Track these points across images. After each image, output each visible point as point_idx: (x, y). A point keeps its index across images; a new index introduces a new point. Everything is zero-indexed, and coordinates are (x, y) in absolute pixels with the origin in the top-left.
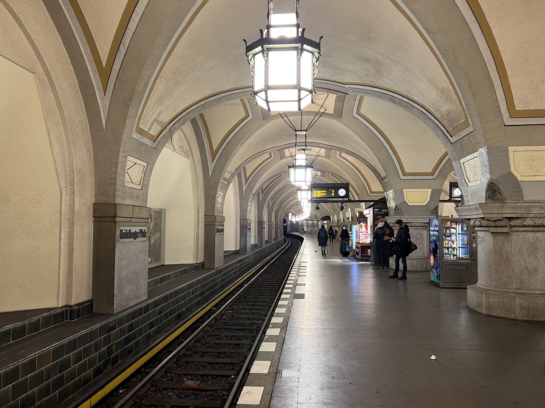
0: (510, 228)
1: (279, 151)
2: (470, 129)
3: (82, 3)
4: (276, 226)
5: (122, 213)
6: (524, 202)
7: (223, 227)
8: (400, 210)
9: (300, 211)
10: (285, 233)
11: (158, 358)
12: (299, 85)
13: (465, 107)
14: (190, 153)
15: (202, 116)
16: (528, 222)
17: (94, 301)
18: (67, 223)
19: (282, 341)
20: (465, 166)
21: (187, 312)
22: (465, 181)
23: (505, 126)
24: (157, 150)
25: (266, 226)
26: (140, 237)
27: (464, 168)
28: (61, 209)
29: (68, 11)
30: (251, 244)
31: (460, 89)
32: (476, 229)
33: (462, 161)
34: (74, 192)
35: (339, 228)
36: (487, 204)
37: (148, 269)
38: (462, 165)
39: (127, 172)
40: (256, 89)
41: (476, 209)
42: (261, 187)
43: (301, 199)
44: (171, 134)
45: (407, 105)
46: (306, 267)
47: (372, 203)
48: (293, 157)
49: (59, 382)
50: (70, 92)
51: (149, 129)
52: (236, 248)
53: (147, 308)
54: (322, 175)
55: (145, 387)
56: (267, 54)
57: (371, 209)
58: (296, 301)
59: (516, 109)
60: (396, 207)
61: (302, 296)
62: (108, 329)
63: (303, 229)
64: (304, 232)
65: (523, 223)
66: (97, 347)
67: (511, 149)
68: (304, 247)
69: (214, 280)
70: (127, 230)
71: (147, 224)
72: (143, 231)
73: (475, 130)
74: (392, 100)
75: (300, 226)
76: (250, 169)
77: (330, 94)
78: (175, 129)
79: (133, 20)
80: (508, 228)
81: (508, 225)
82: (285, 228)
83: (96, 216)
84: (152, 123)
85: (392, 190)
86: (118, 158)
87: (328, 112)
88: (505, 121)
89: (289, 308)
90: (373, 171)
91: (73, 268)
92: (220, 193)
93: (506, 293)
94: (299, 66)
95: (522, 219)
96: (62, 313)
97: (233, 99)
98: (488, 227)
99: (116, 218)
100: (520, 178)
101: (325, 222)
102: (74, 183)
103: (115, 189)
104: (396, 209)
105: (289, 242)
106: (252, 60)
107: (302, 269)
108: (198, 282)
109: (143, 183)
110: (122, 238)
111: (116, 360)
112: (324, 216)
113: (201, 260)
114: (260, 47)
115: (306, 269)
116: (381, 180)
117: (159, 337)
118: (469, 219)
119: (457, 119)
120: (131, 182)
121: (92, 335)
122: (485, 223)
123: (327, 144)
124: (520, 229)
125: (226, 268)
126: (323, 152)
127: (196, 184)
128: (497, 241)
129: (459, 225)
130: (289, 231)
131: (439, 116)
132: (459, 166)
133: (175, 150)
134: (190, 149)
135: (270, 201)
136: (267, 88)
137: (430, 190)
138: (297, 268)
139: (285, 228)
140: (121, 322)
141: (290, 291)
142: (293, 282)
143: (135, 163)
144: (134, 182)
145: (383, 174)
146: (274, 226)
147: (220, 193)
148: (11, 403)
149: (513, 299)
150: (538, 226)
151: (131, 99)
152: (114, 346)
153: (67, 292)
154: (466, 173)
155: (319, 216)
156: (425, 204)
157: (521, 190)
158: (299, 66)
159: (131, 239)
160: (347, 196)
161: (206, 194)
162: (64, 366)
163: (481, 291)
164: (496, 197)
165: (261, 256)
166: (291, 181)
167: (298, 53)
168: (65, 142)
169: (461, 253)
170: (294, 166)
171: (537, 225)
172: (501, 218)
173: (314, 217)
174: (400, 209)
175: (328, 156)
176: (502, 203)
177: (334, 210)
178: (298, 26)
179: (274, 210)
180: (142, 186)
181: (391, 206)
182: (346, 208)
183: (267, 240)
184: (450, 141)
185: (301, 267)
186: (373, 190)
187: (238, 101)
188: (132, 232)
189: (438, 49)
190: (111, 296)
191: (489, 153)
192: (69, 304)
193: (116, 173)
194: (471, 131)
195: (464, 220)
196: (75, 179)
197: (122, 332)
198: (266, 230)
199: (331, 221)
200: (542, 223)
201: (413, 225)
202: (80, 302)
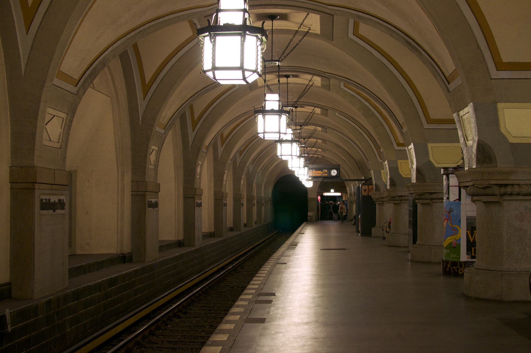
15: (135, 46)
24: (79, 96)
25: (229, 201)
39: (46, 128)
42: (220, 134)
54: (322, 114)
72: (62, 201)
92: (153, 147)
94: (280, 123)
126: (317, 81)
135: (238, 156)
143: (53, 116)
144: (52, 140)
148: (4, 346)
158: (280, 123)
159: (51, 211)
166: (278, 155)
167: (279, 117)
191: (476, 110)
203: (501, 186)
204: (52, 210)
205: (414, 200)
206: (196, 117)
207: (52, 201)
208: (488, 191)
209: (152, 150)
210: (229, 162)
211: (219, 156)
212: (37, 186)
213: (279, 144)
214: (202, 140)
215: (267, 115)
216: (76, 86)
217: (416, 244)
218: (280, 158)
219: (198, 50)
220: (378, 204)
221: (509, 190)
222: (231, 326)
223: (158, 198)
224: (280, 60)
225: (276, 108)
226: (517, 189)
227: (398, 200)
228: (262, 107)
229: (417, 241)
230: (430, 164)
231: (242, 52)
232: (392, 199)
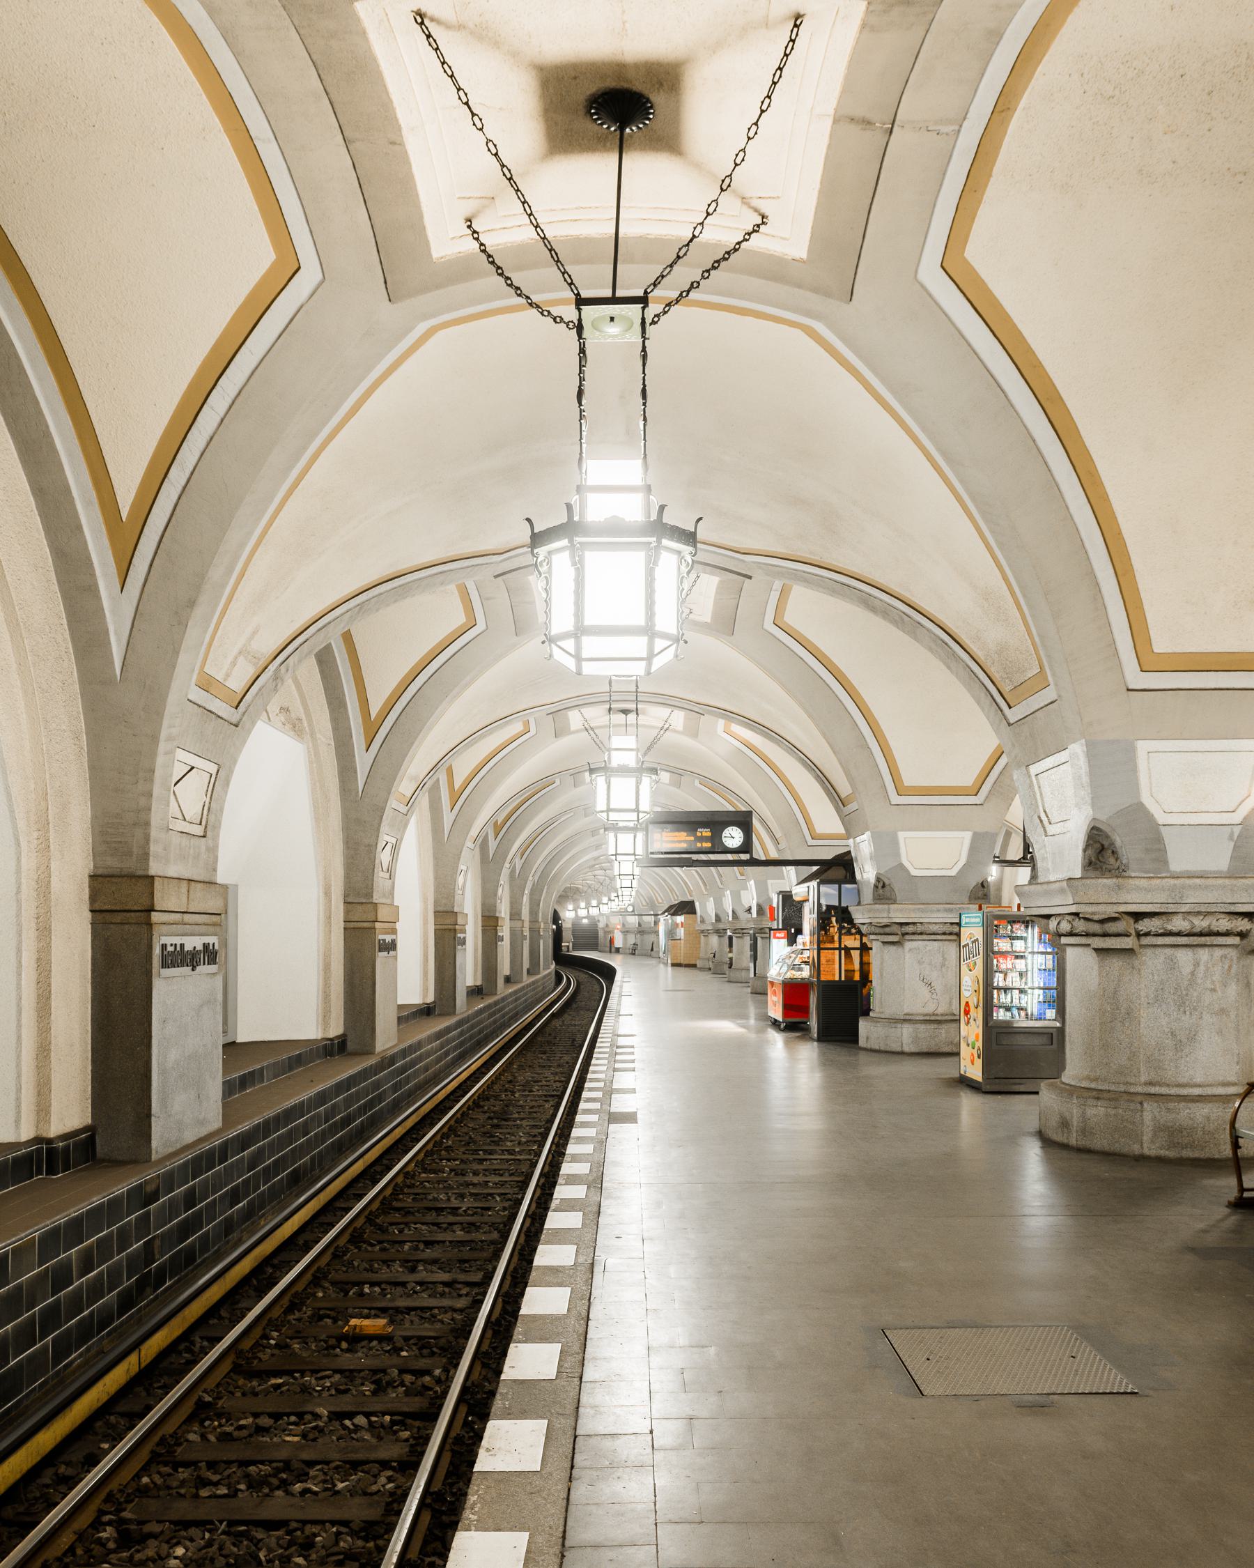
0: (1136, 938)
1: (551, 716)
2: (1049, 694)
3: (79, 361)
4: (534, 932)
5: (167, 898)
6: (1168, 875)
7: (393, 937)
8: (887, 888)
9: (607, 887)
10: (561, 958)
11: (265, 1276)
12: (653, 625)
13: (1037, 639)
14: (305, 724)
15: (348, 638)
16: (1178, 924)
17: (100, 1130)
18: (33, 925)
19: (595, 1209)
20: (1041, 783)
21: (312, 1169)
22: (1041, 821)
23: (1128, 690)
25: (505, 931)
26: (204, 964)
27: (1040, 787)
28: (18, 892)
29: (40, 379)
30: (400, 1002)
31: (1024, 596)
32: (1064, 940)
33: (1034, 769)
34: (49, 847)
35: (722, 939)
36: (1084, 881)
37: (224, 1046)
38: (1034, 778)
40: (555, 630)
41: (1062, 891)
44: (277, 685)
45: (902, 620)
46: (633, 1047)
47: (815, 868)
48: (591, 732)
49: (51, 1318)
50: (35, 583)
51: (228, 675)
52: (425, 995)
53: (224, 1151)
55: (252, 1335)
57: (814, 884)
58: (612, 1127)
59: (1155, 651)
60: (878, 880)
61: (630, 1118)
62: (143, 1196)
63: (611, 941)
64: (613, 950)
65: (1165, 925)
66: (124, 1239)
67: (1142, 747)
68: (620, 995)
69: (377, 1085)
70: (176, 945)
71: (218, 928)
72: (211, 948)
73: (1059, 696)
74: (867, 603)
75: (601, 934)
76: (463, 767)
77: (702, 575)
78: (287, 670)
79: (212, 408)
80: (1132, 937)
81: (1133, 932)
82: (558, 936)
83: (97, 909)
84: (236, 658)
85: (868, 833)
86: (153, 755)
87: (697, 618)
89: (601, 1144)
90: (817, 778)
91: (50, 1043)
92: (387, 838)
93: (1125, 1095)
95: (1164, 917)
96: (29, 1156)
97: (442, 584)
98: (1087, 935)
99: (153, 913)
100: (1161, 818)
101: (680, 919)
102: (48, 824)
103: (147, 840)
104: (877, 887)
105: (571, 978)
106: (545, 564)
107: (621, 1054)
108: (340, 1087)
109: (207, 819)
110: (164, 965)
111: (161, 1276)
112: (677, 902)
113: (336, 1029)
114: (566, 540)
115: (633, 1053)
116: (840, 803)
117: (262, 1223)
118: (1048, 917)
119: (1021, 666)
120: (181, 817)
121: (112, 1209)
122: (1080, 926)
123: (691, 699)
124: (1160, 941)
125: (404, 1053)
126: (678, 719)
127: (319, 816)
128: (1108, 969)
129: (1033, 927)
130: (568, 947)
131: (980, 654)
132: (1028, 781)
134: (305, 713)
136: (580, 631)
137: (967, 836)
138: (608, 1050)
139: (558, 936)
140: (169, 1181)
141: (597, 1106)
142: (601, 1085)
143: (190, 768)
145: (844, 789)
146: (527, 933)
147: (386, 837)
149: (1139, 1108)
150: (1201, 934)
151: (192, 604)
152: (158, 1242)
153: (38, 1104)
154: (1042, 799)
156: (953, 873)
157: (1162, 846)
159: (185, 968)
160: (746, 847)
161: (347, 842)
162: (61, 1277)
163: (1071, 1091)
164: (1104, 863)
165: (495, 1022)
168: (24, 716)
169: (1033, 1001)
170: (605, 769)
171: (1197, 930)
172: (1117, 915)
173: (644, 904)
174: (889, 885)
175: (692, 732)
176: (1117, 877)
178: (648, 489)
179: (529, 885)
180: (206, 827)
181: (865, 877)
182: (743, 878)
183: (479, 983)
184: (1005, 718)
185: (617, 1047)
187: (452, 588)
188: (186, 949)
189: (973, 500)
190: (145, 1116)
191: (1091, 755)
192: (44, 1135)
193: (150, 795)
194: (1052, 700)
195: (1035, 919)
196: (50, 811)
197: (172, 1208)
198: (504, 949)
199: (696, 918)
200: (1209, 926)
201: (919, 928)
202: (67, 1130)
204: (187, 966)
205: (754, 934)
207: (188, 948)
208: (887, 930)
209: (179, 770)
210: (469, 844)
212: (155, 917)
215: (582, 515)
220: (762, 938)
221: (910, 929)
225: (633, 764)
227: (897, 934)
228: (605, 761)
231: (651, 588)
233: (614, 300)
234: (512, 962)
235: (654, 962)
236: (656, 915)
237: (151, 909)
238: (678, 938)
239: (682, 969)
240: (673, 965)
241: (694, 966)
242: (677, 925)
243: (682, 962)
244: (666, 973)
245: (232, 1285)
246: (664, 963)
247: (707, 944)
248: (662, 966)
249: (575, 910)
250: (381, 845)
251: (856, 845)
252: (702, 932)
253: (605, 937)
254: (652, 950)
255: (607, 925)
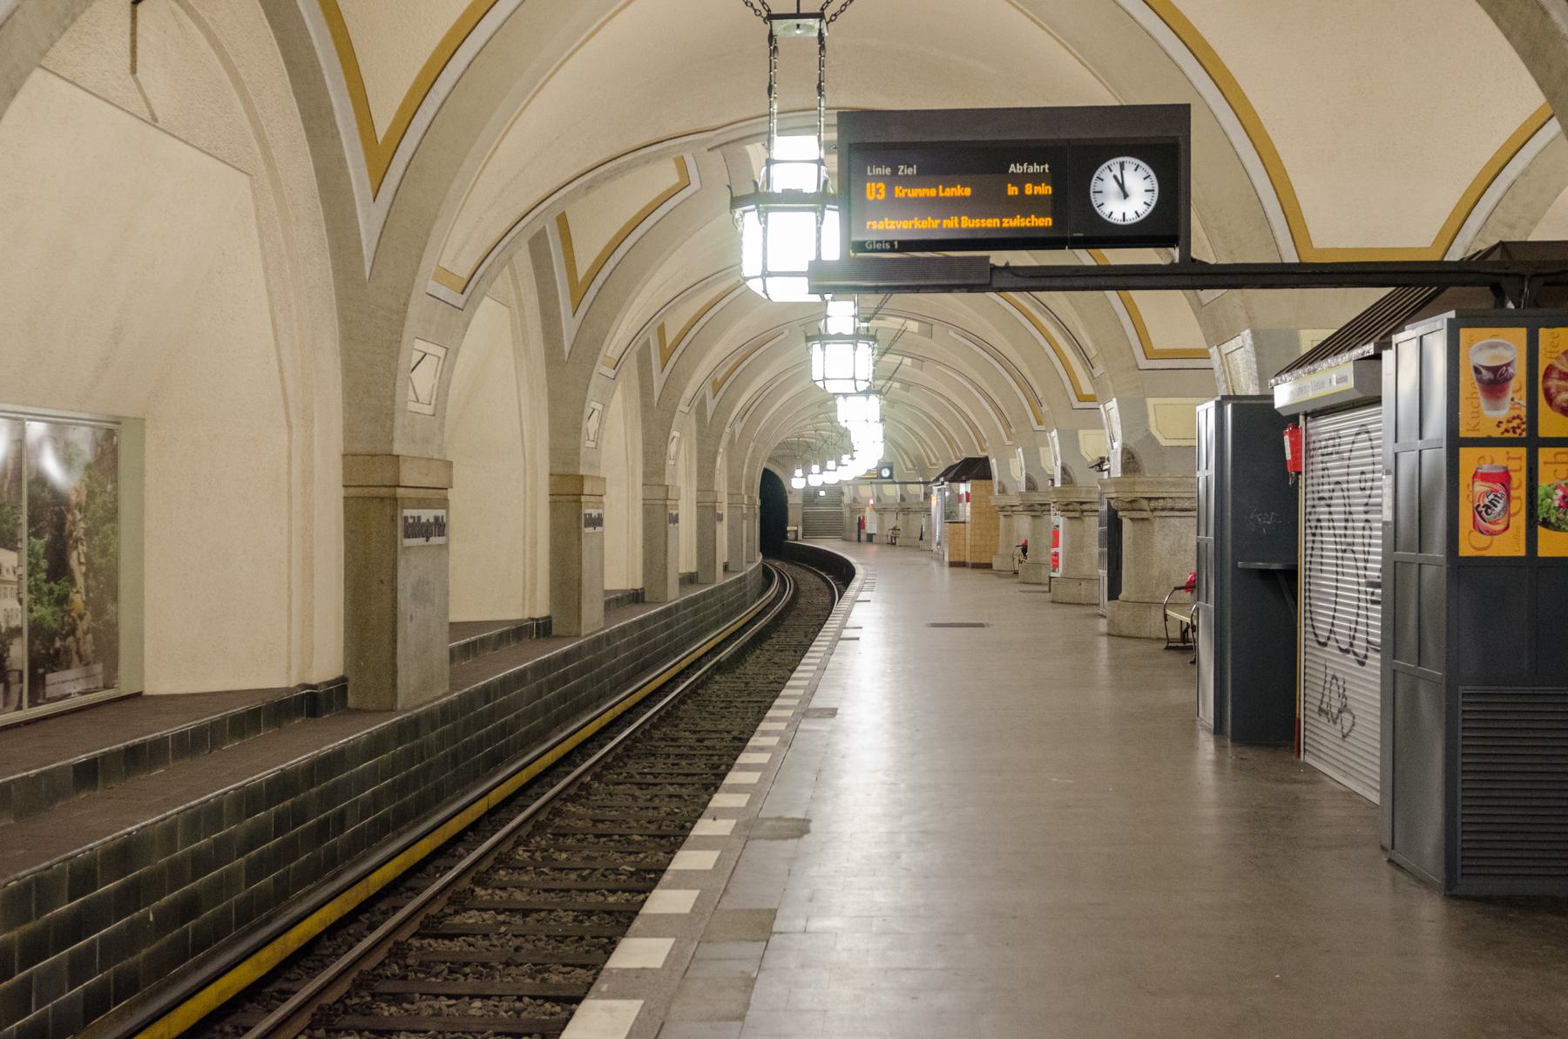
7: (441, 513)
9: (838, 444)
30: (456, 616)
35: (1038, 521)
43: (766, 274)
56: (766, 218)
63: (861, 524)
64: (863, 537)
67: (1081, 433)
75: (847, 513)
88: (1139, 361)
92: (593, 404)
101: (964, 488)
130: (796, 532)
133: (156, 120)
135: (709, 395)
143: (422, 354)
155: (934, 461)
158: (819, 230)
173: (910, 466)
177: (1008, 425)
182: (1011, 443)
183: (693, 570)
186: (1158, 343)
203: (1150, 499)
206: (581, 274)
207: (423, 520)
208: (1071, 507)
209: (416, 356)
210: (682, 407)
211: (567, 349)
212: (583, 499)
213: (756, 213)
214: (597, 344)
216: (462, 293)
217: (1117, 599)
218: (822, 386)
219: (807, 362)
221: (1161, 503)
222: (752, 778)
223: (603, 508)
224: (828, 13)
226: (1169, 504)
229: (1120, 593)
230: (1151, 440)
232: (1128, 506)
233: (798, 15)
234: (730, 550)
235: (922, 559)
236: (926, 483)
237: (581, 494)
238: (963, 520)
239: (968, 571)
240: (952, 564)
241: (989, 566)
242: (959, 498)
243: (968, 560)
244: (942, 576)
245: (184, 1028)
246: (937, 560)
247: (1009, 531)
248: (935, 564)
249: (805, 476)
250: (588, 411)
251: (1501, 257)
252: (1002, 509)
253: (852, 517)
254: (921, 539)
255: (855, 500)
